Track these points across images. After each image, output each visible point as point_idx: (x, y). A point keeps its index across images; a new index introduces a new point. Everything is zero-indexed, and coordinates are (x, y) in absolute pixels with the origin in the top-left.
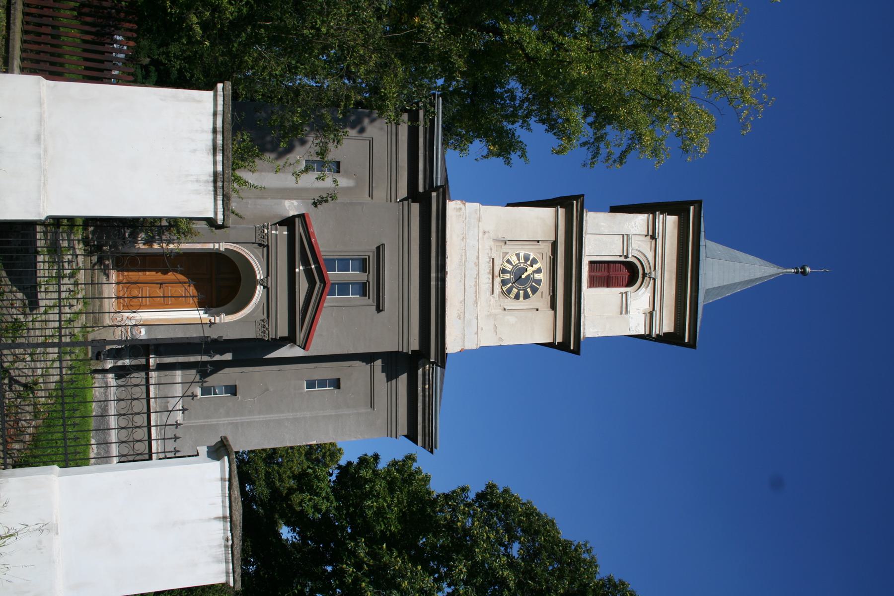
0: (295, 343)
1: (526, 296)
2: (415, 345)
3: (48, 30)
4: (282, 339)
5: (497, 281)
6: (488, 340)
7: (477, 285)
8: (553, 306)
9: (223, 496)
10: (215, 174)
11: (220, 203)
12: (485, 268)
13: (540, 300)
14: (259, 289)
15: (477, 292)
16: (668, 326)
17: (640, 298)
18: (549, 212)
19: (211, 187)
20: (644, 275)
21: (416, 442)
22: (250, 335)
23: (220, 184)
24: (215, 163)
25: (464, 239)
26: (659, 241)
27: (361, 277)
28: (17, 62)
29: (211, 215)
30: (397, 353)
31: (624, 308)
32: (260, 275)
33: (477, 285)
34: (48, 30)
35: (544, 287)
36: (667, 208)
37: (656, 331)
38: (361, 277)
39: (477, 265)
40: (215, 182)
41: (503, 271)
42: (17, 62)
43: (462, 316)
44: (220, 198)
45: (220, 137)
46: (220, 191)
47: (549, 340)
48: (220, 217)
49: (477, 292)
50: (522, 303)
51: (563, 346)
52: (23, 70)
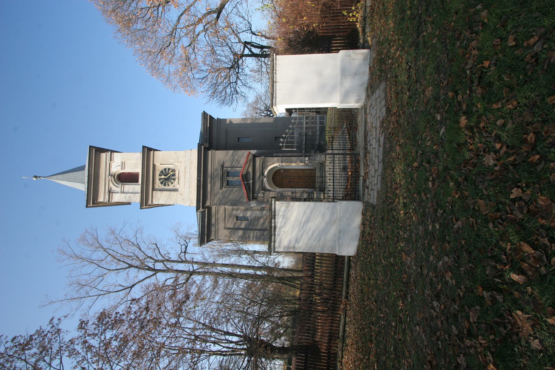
0: (322, 189)
1: (165, 169)
2: (210, 152)
3: (335, 325)
4: (258, 157)
5: (177, 176)
6: (181, 153)
7: (185, 174)
8: (154, 166)
9: (276, 98)
10: (275, 218)
11: (273, 207)
12: (182, 181)
13: (160, 167)
14: (266, 173)
15: (185, 172)
16: (103, 155)
17: (116, 169)
18: (155, 202)
19: (277, 213)
20: (114, 177)
21: (210, 116)
22: (269, 159)
23: (273, 214)
24: (275, 223)
25: (190, 192)
26: (107, 191)
27: (230, 179)
28: (346, 260)
29: (277, 202)
30: (217, 150)
31: (123, 165)
32: (265, 179)
33: (185, 174)
34: (335, 325)
35: (158, 173)
36: (103, 204)
37: (109, 153)
38: (230, 179)
39: (185, 182)
40: (275, 215)
41: (174, 179)
42: (346, 260)
43: (191, 163)
44: (273, 209)
45: (273, 233)
46: (273, 212)
47: (155, 152)
48: (273, 202)
49: (185, 172)
50: (167, 166)
51: (150, 149)
52: (344, 257)
